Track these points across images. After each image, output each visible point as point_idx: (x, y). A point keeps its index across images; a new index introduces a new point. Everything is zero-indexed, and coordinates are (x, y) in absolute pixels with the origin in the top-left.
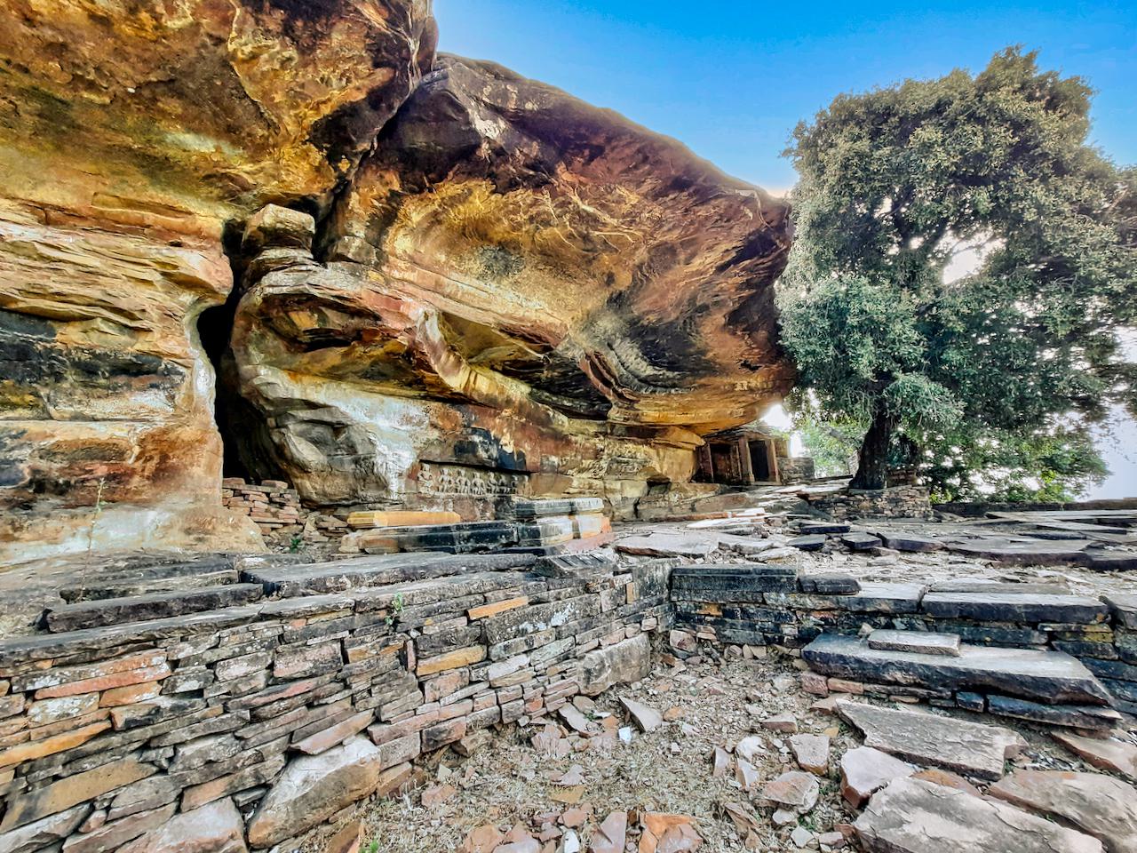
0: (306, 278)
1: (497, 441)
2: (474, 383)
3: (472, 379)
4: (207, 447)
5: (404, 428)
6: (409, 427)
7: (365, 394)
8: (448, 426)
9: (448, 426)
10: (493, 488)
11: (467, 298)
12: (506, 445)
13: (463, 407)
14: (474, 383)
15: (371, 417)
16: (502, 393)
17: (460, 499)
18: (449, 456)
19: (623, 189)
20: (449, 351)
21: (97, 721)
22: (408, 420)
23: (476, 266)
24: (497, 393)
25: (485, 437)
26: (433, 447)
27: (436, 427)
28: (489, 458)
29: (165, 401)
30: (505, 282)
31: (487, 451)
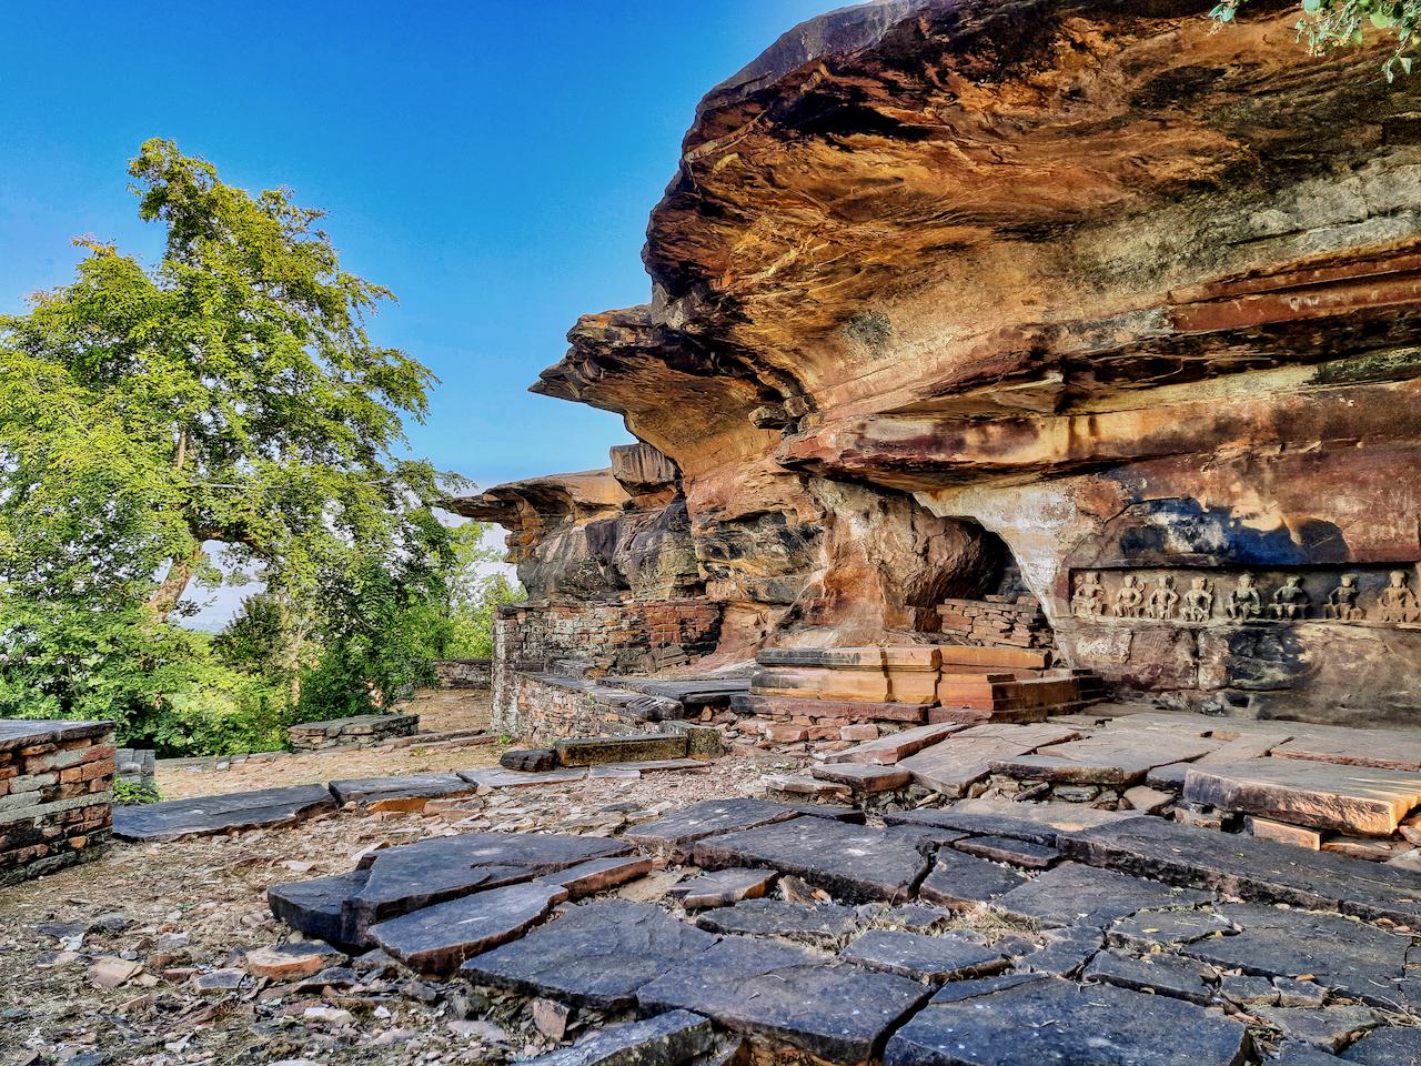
4: (869, 580)
5: (1049, 524)
6: (1054, 523)
7: (999, 492)
8: (1103, 508)
9: (1103, 508)
10: (1245, 607)
11: (880, 387)
13: (1120, 472)
15: (1009, 519)
17: (1145, 628)
18: (1113, 556)
19: (737, 246)
21: (583, 755)
22: (1049, 512)
23: (861, 349)
24: (1175, 426)
25: (1182, 512)
26: (1085, 547)
27: (1088, 514)
30: (895, 342)
31: (1191, 538)
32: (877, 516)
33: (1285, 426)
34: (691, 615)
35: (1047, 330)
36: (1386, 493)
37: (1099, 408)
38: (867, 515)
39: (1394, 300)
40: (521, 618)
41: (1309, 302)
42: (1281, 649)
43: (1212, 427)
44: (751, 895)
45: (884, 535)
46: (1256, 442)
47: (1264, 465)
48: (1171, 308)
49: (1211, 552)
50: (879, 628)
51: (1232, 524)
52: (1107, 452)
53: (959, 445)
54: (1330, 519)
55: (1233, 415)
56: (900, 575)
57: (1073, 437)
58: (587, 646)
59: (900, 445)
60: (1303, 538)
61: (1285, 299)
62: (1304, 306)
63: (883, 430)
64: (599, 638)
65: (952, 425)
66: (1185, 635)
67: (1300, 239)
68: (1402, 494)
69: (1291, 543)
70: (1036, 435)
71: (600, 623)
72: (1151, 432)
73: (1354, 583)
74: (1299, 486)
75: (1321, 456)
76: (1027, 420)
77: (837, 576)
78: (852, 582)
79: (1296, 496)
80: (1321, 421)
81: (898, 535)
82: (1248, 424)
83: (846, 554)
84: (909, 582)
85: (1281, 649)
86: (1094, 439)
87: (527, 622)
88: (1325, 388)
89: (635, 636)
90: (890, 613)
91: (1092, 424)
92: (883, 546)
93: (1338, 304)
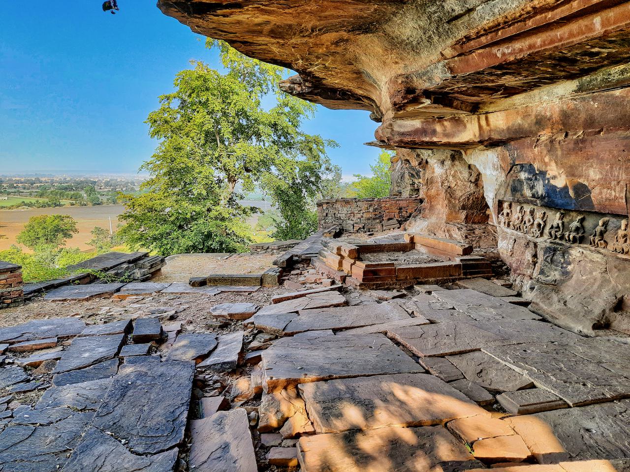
0: (185, 290)
1: (543, 173)
2: (488, 124)
3: (483, 123)
12: (554, 177)
14: (488, 124)
16: (526, 115)
20: (439, 122)
24: (519, 121)
25: (530, 173)
28: (533, 196)
29: (191, 287)
31: (532, 188)
32: (448, 163)
33: (566, 122)
34: (405, 205)
35: (407, 78)
36: (612, 168)
37: (490, 110)
38: (443, 162)
39: (549, 44)
40: (325, 206)
41: (506, 51)
42: (562, 260)
43: (535, 121)
44: (538, 320)
45: (452, 172)
46: (554, 131)
47: (557, 146)
48: (446, 61)
49: (538, 198)
50: (444, 221)
51: (547, 181)
52: (496, 137)
53: (434, 132)
54: (586, 183)
55: (543, 113)
56: (459, 194)
57: (480, 127)
58: (353, 219)
59: (409, 134)
60: (575, 194)
61: (494, 50)
62: (504, 54)
63: (400, 126)
64: (359, 216)
65: (429, 122)
66: (532, 245)
67: (474, 15)
68: (620, 169)
69: (570, 197)
70: (465, 126)
71: (359, 209)
72: (510, 124)
73: (605, 224)
74: (573, 160)
75: (583, 141)
76: (459, 118)
77: (429, 194)
78: (434, 197)
79: (571, 167)
80: (583, 116)
81: (460, 172)
82: (549, 120)
83: (432, 183)
84: (464, 197)
85: (562, 260)
86: (488, 128)
87: (327, 208)
88: (584, 95)
89: (376, 215)
90: (450, 214)
91: (487, 118)
92: (451, 178)
93: (521, 50)
